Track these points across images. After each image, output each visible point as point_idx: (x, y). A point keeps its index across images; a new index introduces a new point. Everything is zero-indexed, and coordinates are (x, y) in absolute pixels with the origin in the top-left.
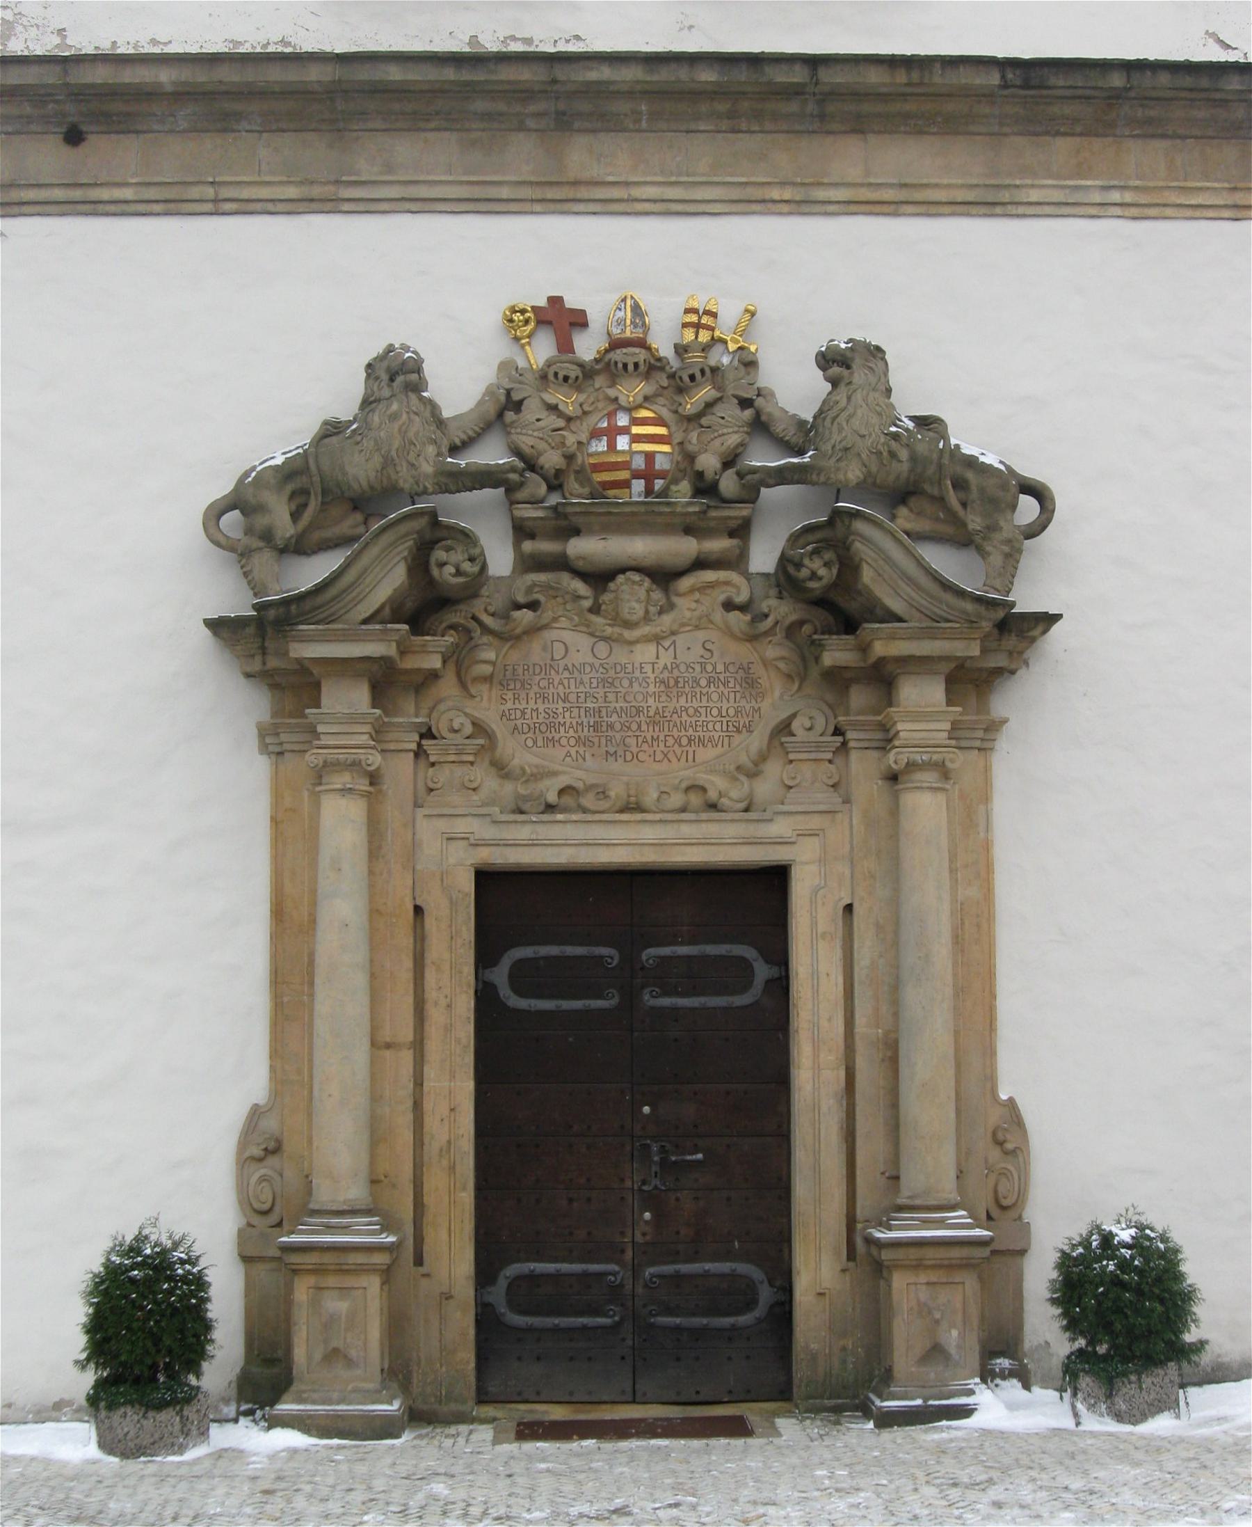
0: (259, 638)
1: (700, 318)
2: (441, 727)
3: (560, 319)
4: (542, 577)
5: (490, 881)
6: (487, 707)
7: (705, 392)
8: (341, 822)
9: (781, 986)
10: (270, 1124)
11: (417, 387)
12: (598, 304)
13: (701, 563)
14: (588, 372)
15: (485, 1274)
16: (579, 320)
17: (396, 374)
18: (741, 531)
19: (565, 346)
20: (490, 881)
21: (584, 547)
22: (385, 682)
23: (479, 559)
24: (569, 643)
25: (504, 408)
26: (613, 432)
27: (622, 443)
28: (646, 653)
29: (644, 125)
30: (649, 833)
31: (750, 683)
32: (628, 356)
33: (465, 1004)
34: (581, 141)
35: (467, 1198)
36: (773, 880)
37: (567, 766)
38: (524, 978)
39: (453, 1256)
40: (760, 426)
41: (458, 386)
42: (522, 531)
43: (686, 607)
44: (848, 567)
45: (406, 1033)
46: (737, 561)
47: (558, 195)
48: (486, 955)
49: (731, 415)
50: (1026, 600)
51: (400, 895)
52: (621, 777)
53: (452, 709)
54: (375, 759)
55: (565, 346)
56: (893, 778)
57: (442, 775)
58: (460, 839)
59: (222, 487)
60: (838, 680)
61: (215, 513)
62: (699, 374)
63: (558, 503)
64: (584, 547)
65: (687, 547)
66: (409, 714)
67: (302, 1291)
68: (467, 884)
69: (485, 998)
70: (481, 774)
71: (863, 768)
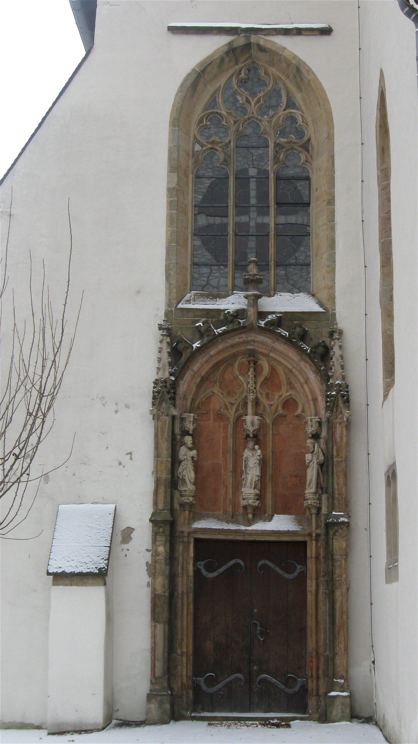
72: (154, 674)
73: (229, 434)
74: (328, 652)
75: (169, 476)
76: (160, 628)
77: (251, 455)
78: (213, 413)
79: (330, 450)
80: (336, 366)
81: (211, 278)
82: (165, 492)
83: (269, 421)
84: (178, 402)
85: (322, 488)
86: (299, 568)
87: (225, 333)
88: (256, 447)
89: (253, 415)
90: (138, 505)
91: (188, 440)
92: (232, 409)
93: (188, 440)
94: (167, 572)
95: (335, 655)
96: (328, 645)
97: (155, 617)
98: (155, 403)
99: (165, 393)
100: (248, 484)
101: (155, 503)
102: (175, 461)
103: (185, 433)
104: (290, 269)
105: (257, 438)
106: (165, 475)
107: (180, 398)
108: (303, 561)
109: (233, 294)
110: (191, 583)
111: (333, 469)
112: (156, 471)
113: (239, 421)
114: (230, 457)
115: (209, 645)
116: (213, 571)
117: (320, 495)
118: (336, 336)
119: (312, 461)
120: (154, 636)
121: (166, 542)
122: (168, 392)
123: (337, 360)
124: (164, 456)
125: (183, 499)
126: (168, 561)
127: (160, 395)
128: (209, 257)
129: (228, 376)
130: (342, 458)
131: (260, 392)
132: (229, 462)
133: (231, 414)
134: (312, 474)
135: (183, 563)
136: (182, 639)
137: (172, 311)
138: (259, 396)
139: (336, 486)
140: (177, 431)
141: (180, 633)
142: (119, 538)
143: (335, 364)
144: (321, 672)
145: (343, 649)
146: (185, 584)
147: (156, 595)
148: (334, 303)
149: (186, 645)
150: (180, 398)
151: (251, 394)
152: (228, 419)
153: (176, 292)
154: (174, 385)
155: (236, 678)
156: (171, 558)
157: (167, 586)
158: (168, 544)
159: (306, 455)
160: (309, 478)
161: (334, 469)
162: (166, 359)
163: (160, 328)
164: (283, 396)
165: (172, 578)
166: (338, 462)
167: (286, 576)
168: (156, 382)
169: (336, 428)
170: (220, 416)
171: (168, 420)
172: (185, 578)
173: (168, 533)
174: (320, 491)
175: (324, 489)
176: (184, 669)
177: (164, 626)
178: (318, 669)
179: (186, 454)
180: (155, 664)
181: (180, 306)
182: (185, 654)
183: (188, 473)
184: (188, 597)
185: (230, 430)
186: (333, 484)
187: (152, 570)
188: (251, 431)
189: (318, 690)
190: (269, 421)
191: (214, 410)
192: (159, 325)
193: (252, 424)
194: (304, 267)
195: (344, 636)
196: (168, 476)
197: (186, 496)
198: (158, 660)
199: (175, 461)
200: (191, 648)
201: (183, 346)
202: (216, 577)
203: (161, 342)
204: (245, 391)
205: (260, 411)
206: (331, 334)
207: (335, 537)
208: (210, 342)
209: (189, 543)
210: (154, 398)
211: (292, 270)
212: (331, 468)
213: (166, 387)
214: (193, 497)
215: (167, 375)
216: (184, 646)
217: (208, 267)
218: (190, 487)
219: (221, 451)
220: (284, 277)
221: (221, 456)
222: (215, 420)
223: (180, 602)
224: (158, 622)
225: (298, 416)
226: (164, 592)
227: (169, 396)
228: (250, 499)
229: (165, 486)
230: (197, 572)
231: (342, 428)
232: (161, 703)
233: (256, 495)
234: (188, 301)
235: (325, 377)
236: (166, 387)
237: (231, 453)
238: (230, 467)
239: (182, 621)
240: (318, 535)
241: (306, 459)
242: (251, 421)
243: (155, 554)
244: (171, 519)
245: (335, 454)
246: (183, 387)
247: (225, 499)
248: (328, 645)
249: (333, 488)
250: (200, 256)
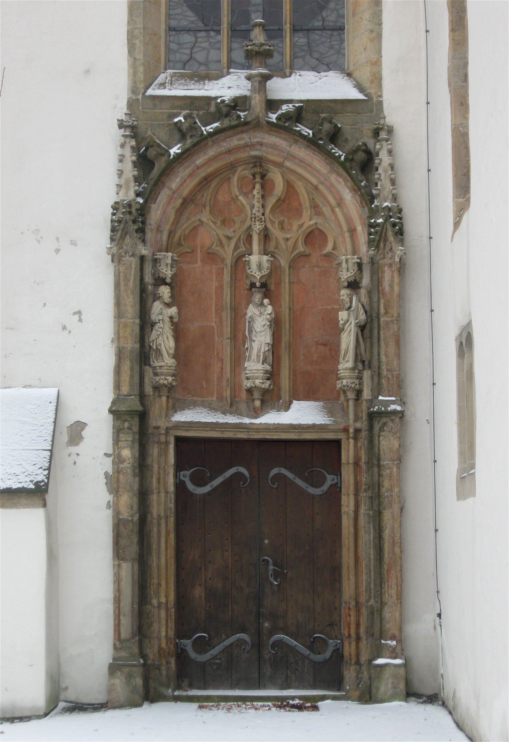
27: (343, 258)
72: (119, 634)
73: (225, 282)
74: (372, 602)
75: (138, 346)
76: (126, 567)
77: (258, 313)
78: (201, 252)
79: (375, 305)
80: (383, 180)
81: (195, 50)
82: (132, 369)
83: (284, 263)
84: (149, 235)
85: (363, 362)
86: (330, 479)
87: (217, 132)
88: (266, 301)
89: (260, 254)
90: (92, 387)
91: (165, 291)
92: (228, 246)
93: (165, 291)
94: (136, 487)
95: (383, 604)
96: (373, 591)
97: (119, 553)
98: (114, 237)
99: (130, 222)
100: (254, 357)
101: (117, 386)
102: (145, 324)
103: (160, 281)
104: (315, 36)
105: (266, 289)
106: (131, 344)
107: (152, 230)
108: (336, 467)
109: (229, 73)
110: (171, 502)
111: (379, 333)
112: (118, 337)
113: (239, 263)
114: (226, 316)
116: (205, 484)
117: (360, 372)
118: (383, 135)
119: (348, 321)
120: (117, 580)
121: (133, 441)
122: (134, 222)
123: (386, 171)
124: (129, 316)
125: (157, 378)
126: (137, 471)
127: (122, 226)
128: (194, 19)
129: (223, 197)
130: (392, 316)
131: (270, 220)
132: (225, 324)
133: (228, 253)
134: (348, 340)
135: (159, 473)
136: (159, 584)
137: (138, 100)
138: (269, 226)
139: (383, 358)
140: (148, 279)
141: (155, 575)
142: (65, 438)
143: (382, 177)
144: (362, 630)
145: (394, 596)
146: (162, 503)
147: (120, 520)
148: (380, 86)
149: (164, 593)
150: (152, 230)
151: (257, 223)
152: (223, 260)
153: (144, 73)
154: (143, 211)
155: (239, 640)
156: (142, 466)
157: (135, 507)
158: (137, 445)
159: (340, 313)
160: (343, 346)
161: (381, 333)
162: (130, 171)
163: (121, 125)
164: (305, 226)
165: (143, 496)
166: (387, 323)
167: (311, 490)
168: (116, 207)
169: (383, 272)
170: (211, 257)
171: (134, 262)
172: (163, 495)
173: (136, 429)
174: (360, 367)
175: (366, 362)
176: (163, 628)
177: (133, 565)
178: (358, 625)
179: (161, 312)
180: (119, 621)
181: (150, 92)
182: (163, 606)
183: (164, 340)
184: (166, 522)
185: (227, 277)
186: (379, 355)
187: (113, 484)
188: (258, 278)
189: (358, 655)
190: (284, 263)
191: (202, 247)
192: (118, 120)
193: (260, 267)
194: (335, 33)
195: (397, 578)
196: (135, 345)
197: (162, 374)
198: (124, 615)
199: (145, 324)
200: (172, 597)
201: (154, 153)
202: (209, 493)
203: (122, 146)
204: (249, 219)
205: (271, 247)
206: (376, 133)
207: (383, 433)
208: (195, 145)
209: (167, 443)
210: (113, 230)
211: (317, 37)
212: (376, 331)
213: (130, 213)
214: (172, 376)
215: (132, 195)
216: (163, 595)
217: (191, 33)
218: (166, 362)
219: (213, 308)
220: (306, 48)
221: (214, 315)
222: (203, 261)
223: (155, 529)
224: (123, 559)
225: (328, 256)
226: (132, 516)
227: (136, 227)
228: (257, 378)
229: (131, 361)
230: (180, 486)
231: (393, 272)
232: (129, 677)
233: (266, 372)
234: (163, 85)
235: (368, 198)
236: (130, 213)
237: (229, 311)
238: (227, 331)
239: (159, 558)
240: (357, 431)
241: (340, 319)
242: (257, 263)
243: (118, 461)
244: (140, 408)
245: (382, 311)
246: (155, 214)
247: (220, 378)
248: (373, 591)
249: (379, 361)
250: (180, 17)
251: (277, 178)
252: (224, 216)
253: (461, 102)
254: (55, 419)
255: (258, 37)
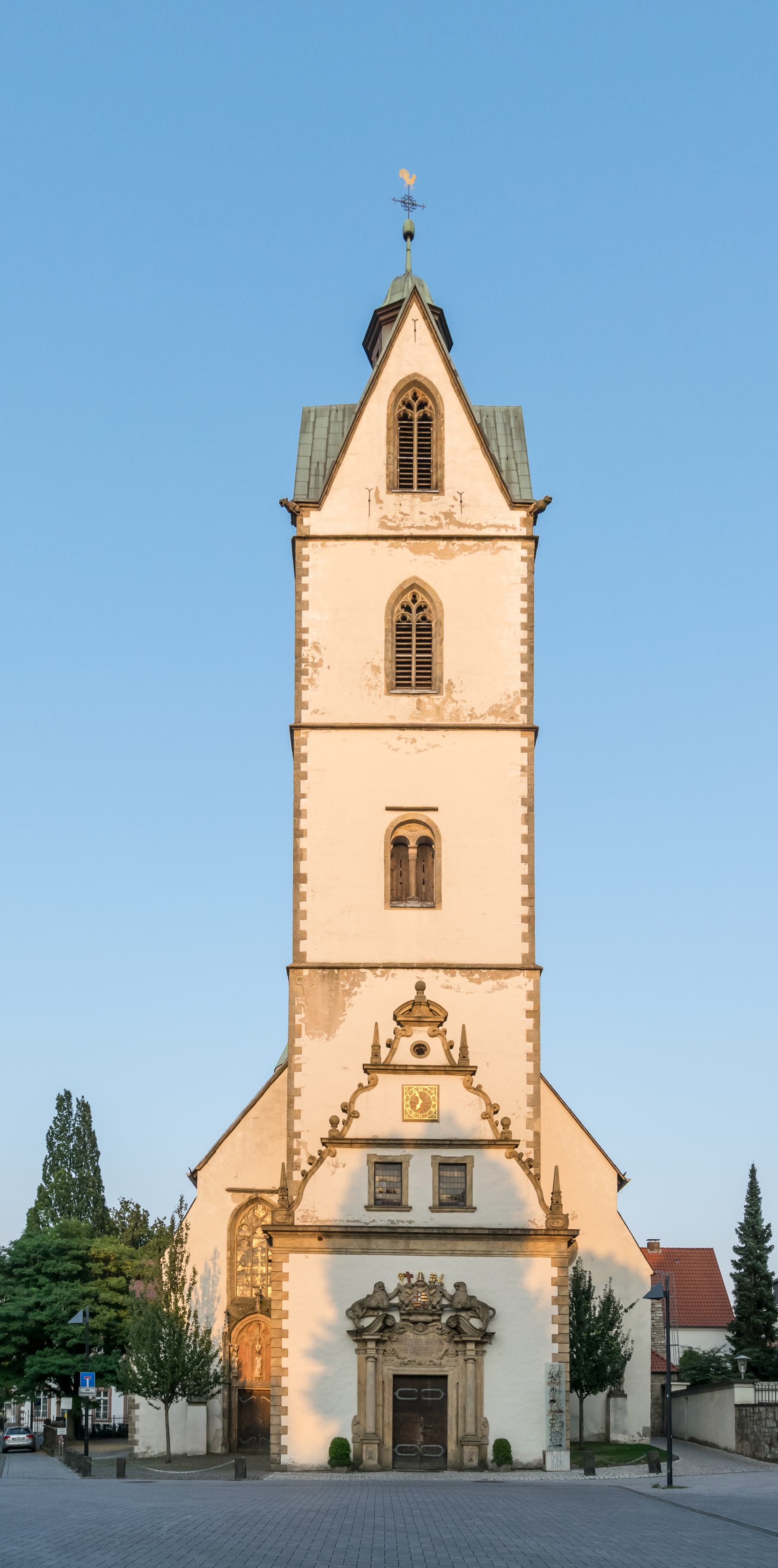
0: (357, 1334)
1: (434, 1276)
2: (387, 1349)
3: (408, 1276)
4: (405, 1323)
5: (396, 1377)
6: (395, 1346)
7: (434, 1290)
8: (370, 1366)
9: (446, 1396)
10: (358, 1419)
11: (384, 1290)
12: (415, 1272)
13: (434, 1321)
14: (413, 1286)
15: (394, 1446)
16: (412, 1276)
17: (380, 1286)
18: (440, 1315)
19: (409, 1281)
20: (396, 1377)
21: (413, 1318)
22: (378, 1342)
23: (394, 1320)
24: (410, 1335)
25: (398, 1292)
26: (418, 1297)
28: (423, 1337)
29: (415, 490)
30: (423, 1369)
31: (441, 1342)
32: (421, 1283)
33: (391, 1398)
34: (412, 1241)
35: (391, 1432)
36: (445, 1377)
37: (409, 1357)
38: (401, 1394)
39: (389, 1441)
40: (443, 1296)
41: (391, 1288)
42: (401, 1314)
43: (430, 1329)
44: (458, 1323)
45: (381, 1403)
46: (439, 1320)
47: (408, 1252)
48: (394, 1390)
49: (438, 1295)
50: (490, 1329)
51: (380, 1378)
52: (418, 1359)
53: (389, 1347)
54: (376, 1356)
55: (409, 1281)
56: (466, 1360)
57: (388, 1358)
58: (390, 1369)
59: (349, 1306)
60: (457, 1342)
61: (347, 1311)
62: (434, 1286)
63: (408, 1311)
64: (413, 1318)
65: (430, 1318)
66: (381, 1347)
67: (364, 1447)
68: (391, 1377)
69: (394, 1397)
70: (394, 1358)
71: (461, 1358)
91: (235, 1354)
105: (259, 1353)
113: (253, 1346)
115: (243, 1427)
129: (250, 1329)
133: (251, 1344)
146: (235, 1405)
149: (235, 1426)
154: (230, 1334)
165: (230, 1403)
170: (247, 1344)
176: (235, 1435)
230: (239, 1401)
242: (258, 1347)
246: (233, 1335)
251: (263, 1325)
252: (250, 1334)
253: (460, 538)
254: (298, 897)
255: (416, 415)
